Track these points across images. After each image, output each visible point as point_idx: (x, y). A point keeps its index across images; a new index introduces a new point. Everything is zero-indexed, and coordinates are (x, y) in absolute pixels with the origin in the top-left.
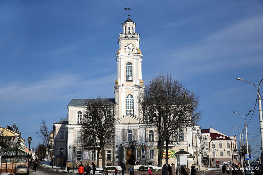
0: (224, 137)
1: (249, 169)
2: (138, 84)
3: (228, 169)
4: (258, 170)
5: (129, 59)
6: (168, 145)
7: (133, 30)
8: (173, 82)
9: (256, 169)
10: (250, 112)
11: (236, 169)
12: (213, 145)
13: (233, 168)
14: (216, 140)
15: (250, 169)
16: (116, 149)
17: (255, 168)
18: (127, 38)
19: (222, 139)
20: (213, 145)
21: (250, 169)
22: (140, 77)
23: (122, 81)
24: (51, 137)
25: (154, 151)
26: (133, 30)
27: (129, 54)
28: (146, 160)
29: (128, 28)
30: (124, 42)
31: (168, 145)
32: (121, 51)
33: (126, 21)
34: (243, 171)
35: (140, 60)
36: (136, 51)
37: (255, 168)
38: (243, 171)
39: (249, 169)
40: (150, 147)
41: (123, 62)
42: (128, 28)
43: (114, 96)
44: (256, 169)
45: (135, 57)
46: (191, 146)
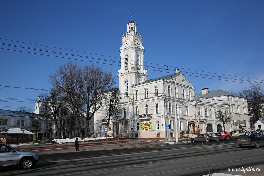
1: (250, 170)
3: (229, 170)
4: (259, 171)
7: (129, 28)
8: (51, 92)
9: (257, 170)
15: (251, 170)
17: (257, 169)
21: (251, 170)
24: (37, 128)
25: (139, 124)
26: (129, 28)
27: (125, 49)
28: (133, 131)
34: (244, 172)
37: (257, 169)
39: (250, 170)
40: (137, 121)
44: (257, 170)
46: (164, 117)
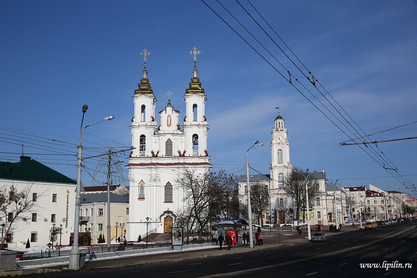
0: (378, 194)
1: (396, 265)
2: (286, 165)
3: (362, 266)
4: (411, 267)
5: (280, 147)
6: (222, 246)
9: (407, 265)
10: (256, 143)
11: (376, 266)
12: (368, 201)
13: (372, 265)
14: (371, 196)
15: (398, 266)
16: (272, 212)
17: (406, 264)
18: (277, 132)
19: (377, 196)
20: (368, 201)
21: (398, 266)
22: (288, 160)
23: (275, 163)
29: (278, 123)
30: (275, 134)
31: (222, 246)
32: (274, 142)
33: (277, 118)
34: (387, 269)
35: (288, 147)
36: (284, 141)
37: (406, 264)
38: (387, 269)
39: (396, 265)
41: (275, 149)
42: (278, 123)
43: (270, 173)
44: (407, 265)
45: (284, 145)
